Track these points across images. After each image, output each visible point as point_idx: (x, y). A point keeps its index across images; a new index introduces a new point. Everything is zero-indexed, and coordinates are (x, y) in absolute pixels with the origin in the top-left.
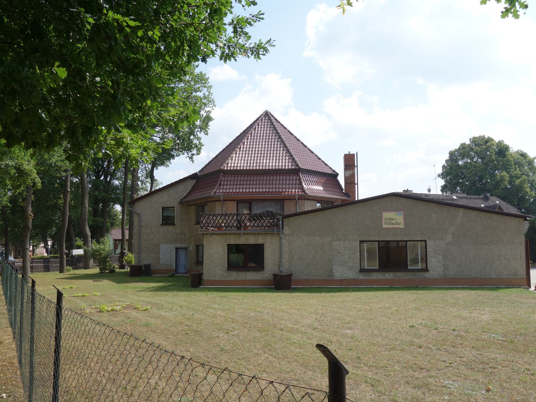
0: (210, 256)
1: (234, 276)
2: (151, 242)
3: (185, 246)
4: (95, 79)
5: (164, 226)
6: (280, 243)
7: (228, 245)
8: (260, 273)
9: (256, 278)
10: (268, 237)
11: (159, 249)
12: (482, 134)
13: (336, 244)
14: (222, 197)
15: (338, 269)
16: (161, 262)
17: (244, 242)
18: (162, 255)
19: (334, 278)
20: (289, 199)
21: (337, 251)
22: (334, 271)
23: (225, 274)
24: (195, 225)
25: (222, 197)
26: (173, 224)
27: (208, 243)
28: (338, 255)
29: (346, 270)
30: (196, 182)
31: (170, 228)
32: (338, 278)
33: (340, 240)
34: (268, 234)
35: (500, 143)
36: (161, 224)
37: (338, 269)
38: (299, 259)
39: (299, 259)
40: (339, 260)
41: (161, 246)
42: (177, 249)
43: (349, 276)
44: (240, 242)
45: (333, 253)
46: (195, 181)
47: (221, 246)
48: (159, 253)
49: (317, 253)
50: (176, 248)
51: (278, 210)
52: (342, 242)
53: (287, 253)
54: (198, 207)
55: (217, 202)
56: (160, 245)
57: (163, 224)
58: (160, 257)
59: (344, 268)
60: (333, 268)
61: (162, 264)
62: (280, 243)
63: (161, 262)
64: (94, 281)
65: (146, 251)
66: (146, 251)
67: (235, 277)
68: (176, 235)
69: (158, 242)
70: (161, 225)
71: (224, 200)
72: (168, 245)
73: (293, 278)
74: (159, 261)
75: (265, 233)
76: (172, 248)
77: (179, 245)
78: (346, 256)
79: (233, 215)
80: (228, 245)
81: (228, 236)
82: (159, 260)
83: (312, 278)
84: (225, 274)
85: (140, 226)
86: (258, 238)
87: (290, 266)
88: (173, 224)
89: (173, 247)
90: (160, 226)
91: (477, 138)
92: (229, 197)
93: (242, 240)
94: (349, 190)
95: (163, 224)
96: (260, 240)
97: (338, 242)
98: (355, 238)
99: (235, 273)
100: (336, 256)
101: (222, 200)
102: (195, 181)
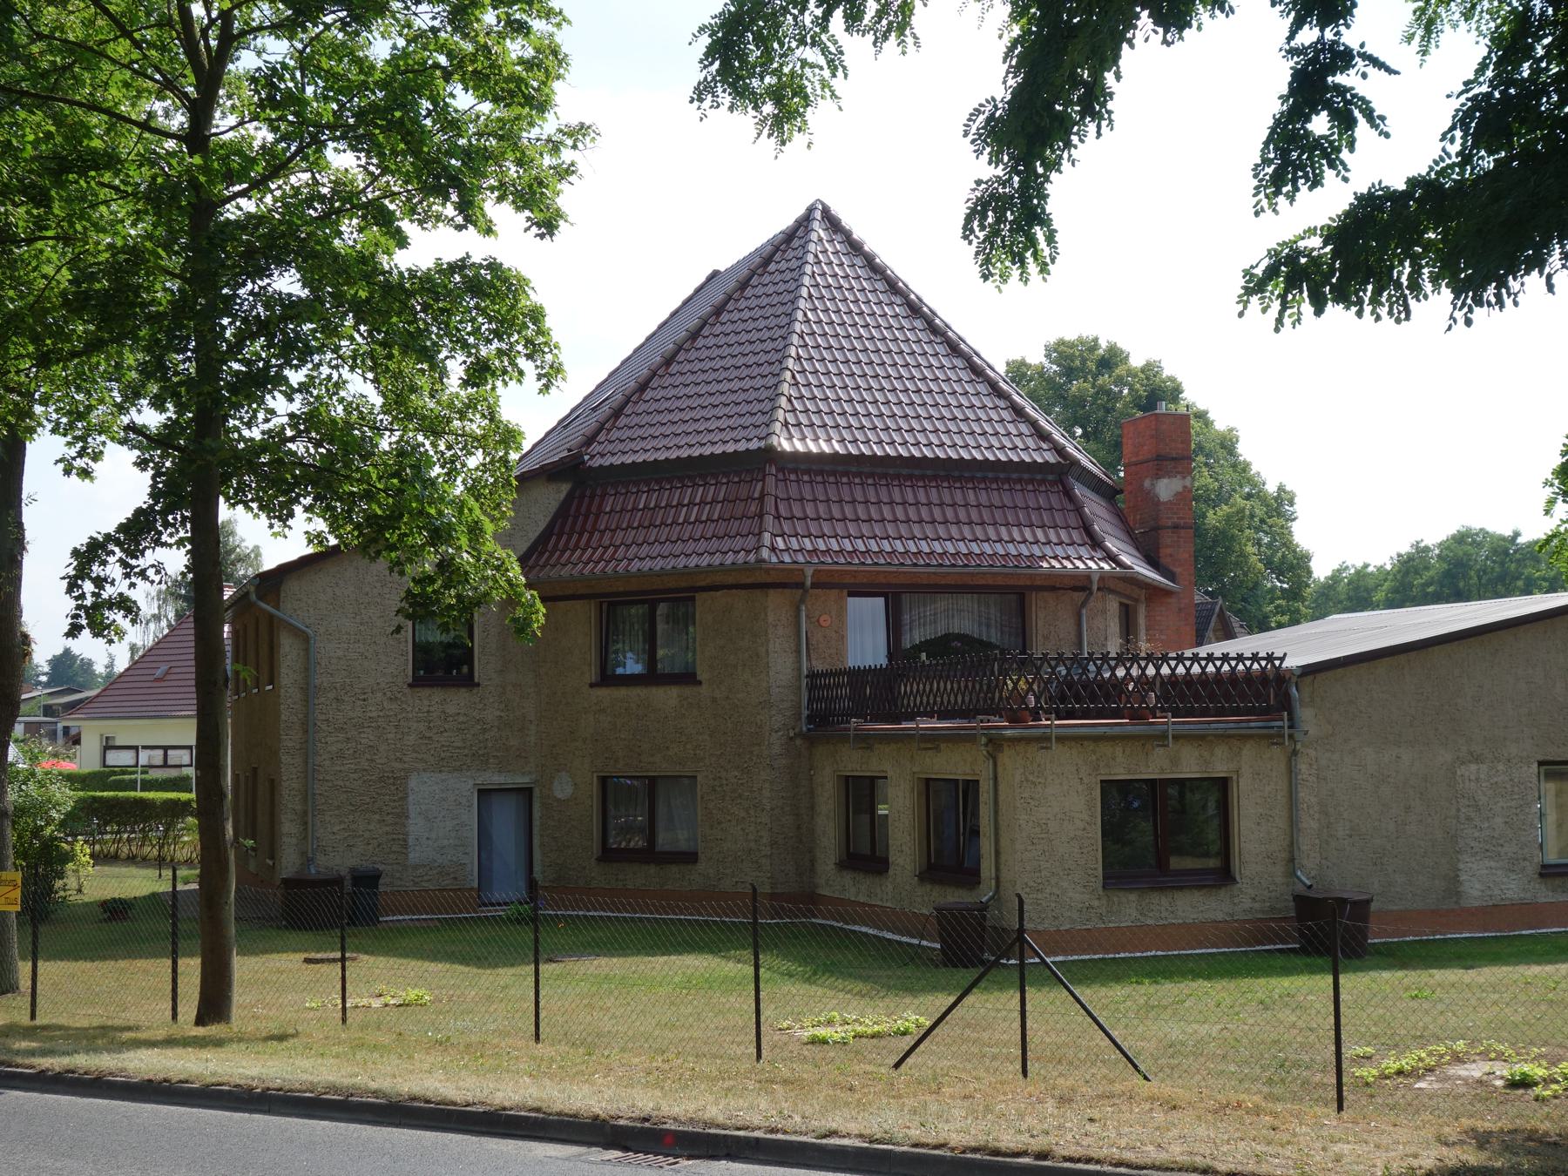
0: (1038, 830)
1: (1130, 910)
2: (365, 765)
3: (522, 780)
4: (1322, 110)
5: (426, 692)
6: (1291, 771)
7: (1106, 785)
8: (1222, 893)
9: (1211, 916)
10: (1248, 751)
11: (404, 798)
12: (1088, 332)
13: (1467, 774)
14: (809, 572)
15: (1475, 867)
16: (411, 856)
17: (1162, 770)
18: (416, 826)
19: (1465, 903)
20: (1053, 589)
21: (1472, 803)
22: (1463, 877)
23: (1096, 903)
24: (592, 686)
25: (809, 572)
26: (469, 682)
27: (1031, 778)
28: (1473, 815)
29: (1499, 872)
30: (570, 497)
31: (455, 701)
32: (1476, 904)
33: (1478, 759)
34: (1250, 737)
35: (1150, 369)
36: (410, 680)
37: (1475, 867)
38: (1351, 836)
39: (1351, 836)
40: (1477, 834)
41: (413, 782)
42: (484, 793)
43: (1509, 894)
44: (1150, 770)
45: (1458, 810)
46: (565, 488)
47: (1080, 788)
48: (403, 815)
49: (1408, 809)
50: (479, 791)
51: (993, 630)
52: (1484, 767)
53: (1311, 812)
54: (605, 606)
55: (771, 591)
56: (406, 778)
57: (417, 683)
58: (407, 834)
59: (1493, 864)
60: (1461, 866)
61: (416, 867)
62: (1291, 771)
63: (414, 856)
64: (308, 961)
65: (338, 807)
66: (338, 807)
67: (1135, 914)
68: (484, 731)
69: (398, 765)
70: (410, 686)
71: (815, 585)
72: (443, 776)
73: (1374, 906)
74: (406, 854)
75: (1240, 735)
76: (465, 786)
77: (495, 779)
78: (1499, 820)
79: (1203, 663)
80: (1106, 785)
81: (1106, 749)
82: (405, 846)
83: (1395, 908)
84: (1096, 903)
85: (308, 691)
86: (1212, 755)
87: (1324, 862)
88: (469, 682)
89: (471, 782)
90: (408, 691)
91: (1072, 345)
92: (878, 572)
93: (1155, 766)
94: (1171, 555)
95: (417, 683)
96: (1219, 767)
97: (1473, 767)
98: (1525, 754)
99: (1133, 897)
100: (1469, 819)
101: (808, 583)
102: (565, 488)
